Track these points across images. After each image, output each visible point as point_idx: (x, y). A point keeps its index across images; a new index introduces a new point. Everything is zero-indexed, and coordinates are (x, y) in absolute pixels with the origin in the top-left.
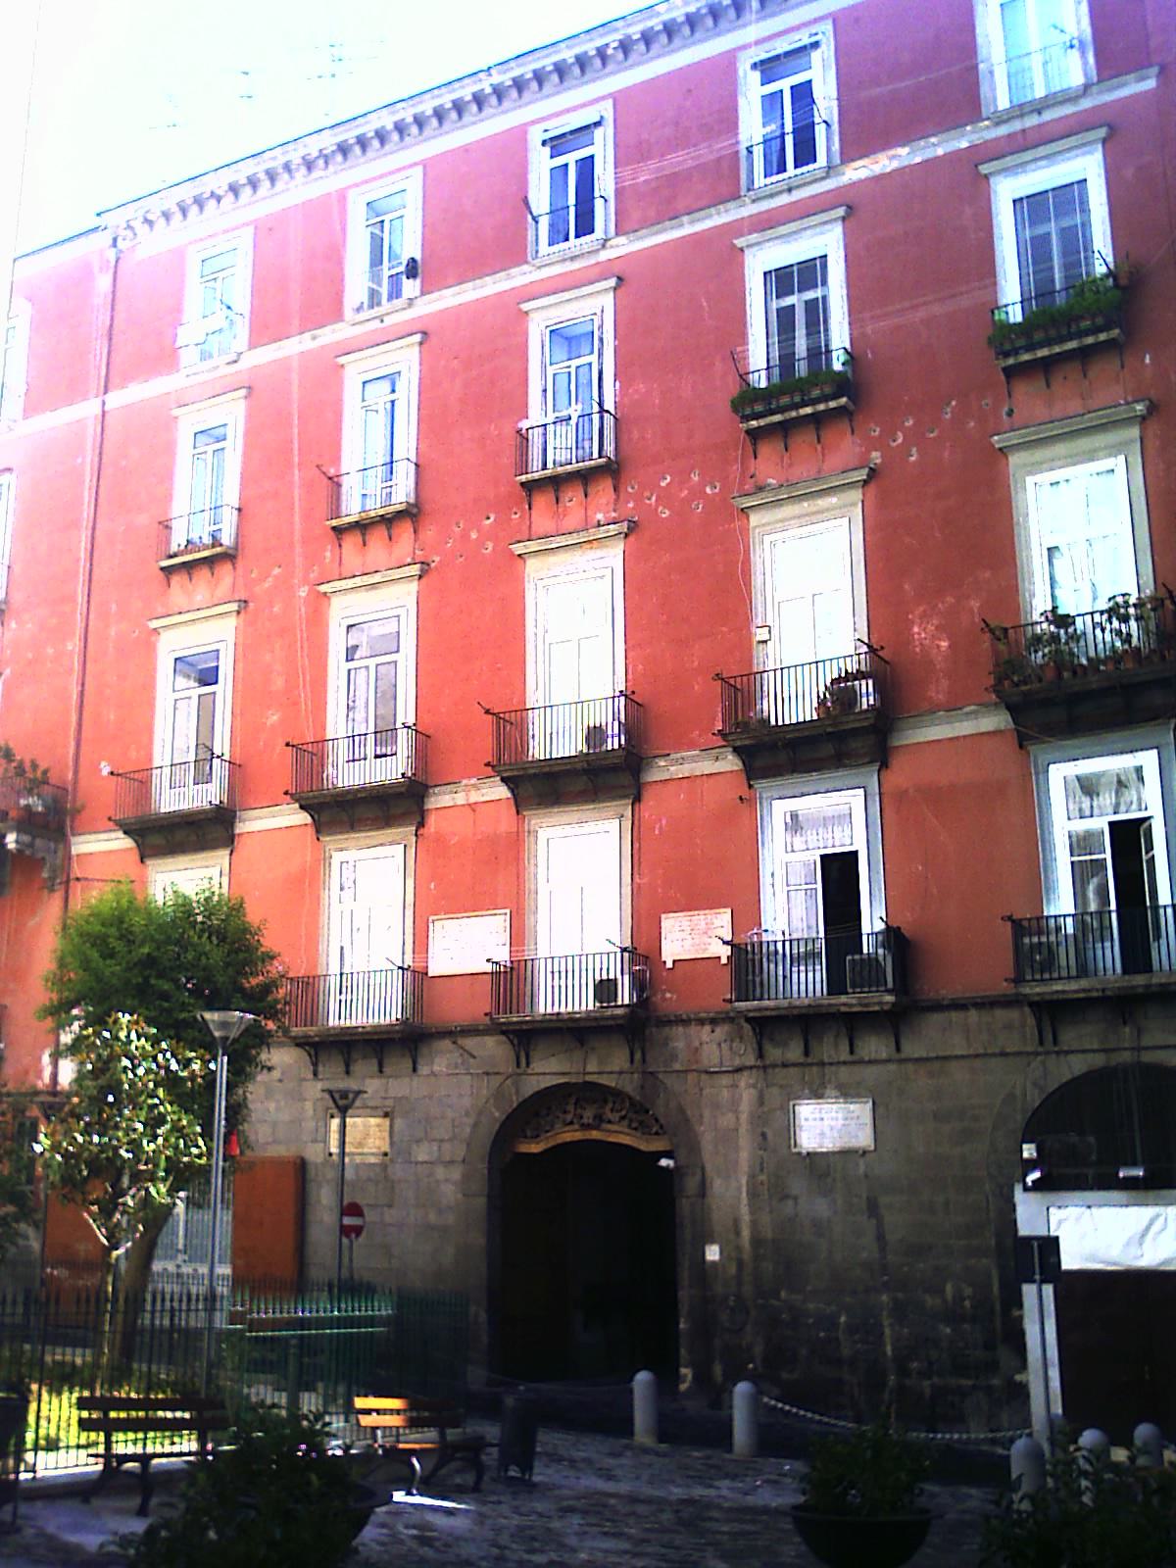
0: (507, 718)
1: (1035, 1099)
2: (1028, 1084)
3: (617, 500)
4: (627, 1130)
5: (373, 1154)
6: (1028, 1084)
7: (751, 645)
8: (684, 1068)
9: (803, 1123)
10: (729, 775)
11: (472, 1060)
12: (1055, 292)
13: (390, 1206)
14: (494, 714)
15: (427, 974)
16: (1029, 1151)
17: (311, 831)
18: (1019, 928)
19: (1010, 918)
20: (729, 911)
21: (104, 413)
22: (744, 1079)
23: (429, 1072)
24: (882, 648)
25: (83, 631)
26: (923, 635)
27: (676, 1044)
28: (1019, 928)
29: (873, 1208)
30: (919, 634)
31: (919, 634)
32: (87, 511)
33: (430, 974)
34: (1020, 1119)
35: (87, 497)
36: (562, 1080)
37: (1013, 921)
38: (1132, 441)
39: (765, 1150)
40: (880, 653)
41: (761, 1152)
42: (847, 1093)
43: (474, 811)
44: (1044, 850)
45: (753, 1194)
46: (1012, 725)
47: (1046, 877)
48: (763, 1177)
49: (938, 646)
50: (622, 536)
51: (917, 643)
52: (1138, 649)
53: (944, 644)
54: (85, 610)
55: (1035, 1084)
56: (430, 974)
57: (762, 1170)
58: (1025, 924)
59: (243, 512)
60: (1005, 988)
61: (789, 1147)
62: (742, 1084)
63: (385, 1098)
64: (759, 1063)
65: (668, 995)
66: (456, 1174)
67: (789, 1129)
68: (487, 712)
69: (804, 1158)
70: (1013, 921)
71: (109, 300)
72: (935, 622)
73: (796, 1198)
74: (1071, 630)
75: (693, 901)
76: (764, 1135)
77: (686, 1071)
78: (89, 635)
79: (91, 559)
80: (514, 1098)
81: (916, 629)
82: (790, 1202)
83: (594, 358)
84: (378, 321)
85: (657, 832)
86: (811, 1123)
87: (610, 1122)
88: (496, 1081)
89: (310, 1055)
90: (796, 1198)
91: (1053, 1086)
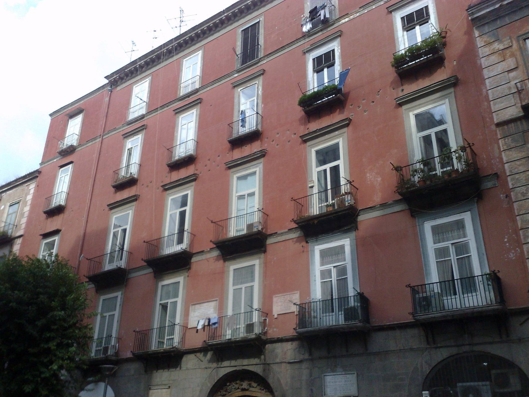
1: (427, 370)
2: (424, 363)
3: (261, 144)
4: (260, 391)
6: (424, 363)
8: (280, 361)
9: (328, 384)
11: (201, 362)
12: (175, 324)
15: (187, 327)
18: (414, 290)
20: (298, 292)
21: (345, 179)
22: (304, 365)
23: (186, 368)
24: (353, 181)
25: (87, 212)
26: (371, 177)
27: (277, 351)
28: (414, 290)
30: (369, 177)
31: (369, 177)
33: (189, 327)
36: (234, 369)
37: (411, 287)
40: (352, 183)
42: (346, 370)
43: (208, 261)
44: (424, 258)
49: (377, 181)
51: (369, 180)
52: (457, 170)
53: (379, 179)
54: (89, 205)
55: (426, 362)
56: (189, 327)
58: (416, 288)
60: (410, 319)
64: (310, 358)
65: (275, 330)
70: (411, 287)
71: (108, 104)
76: (312, 390)
77: (281, 363)
80: (216, 378)
81: (368, 175)
84: (489, 286)
85: (272, 263)
86: (332, 384)
87: (253, 387)
88: (210, 371)
91: (434, 363)
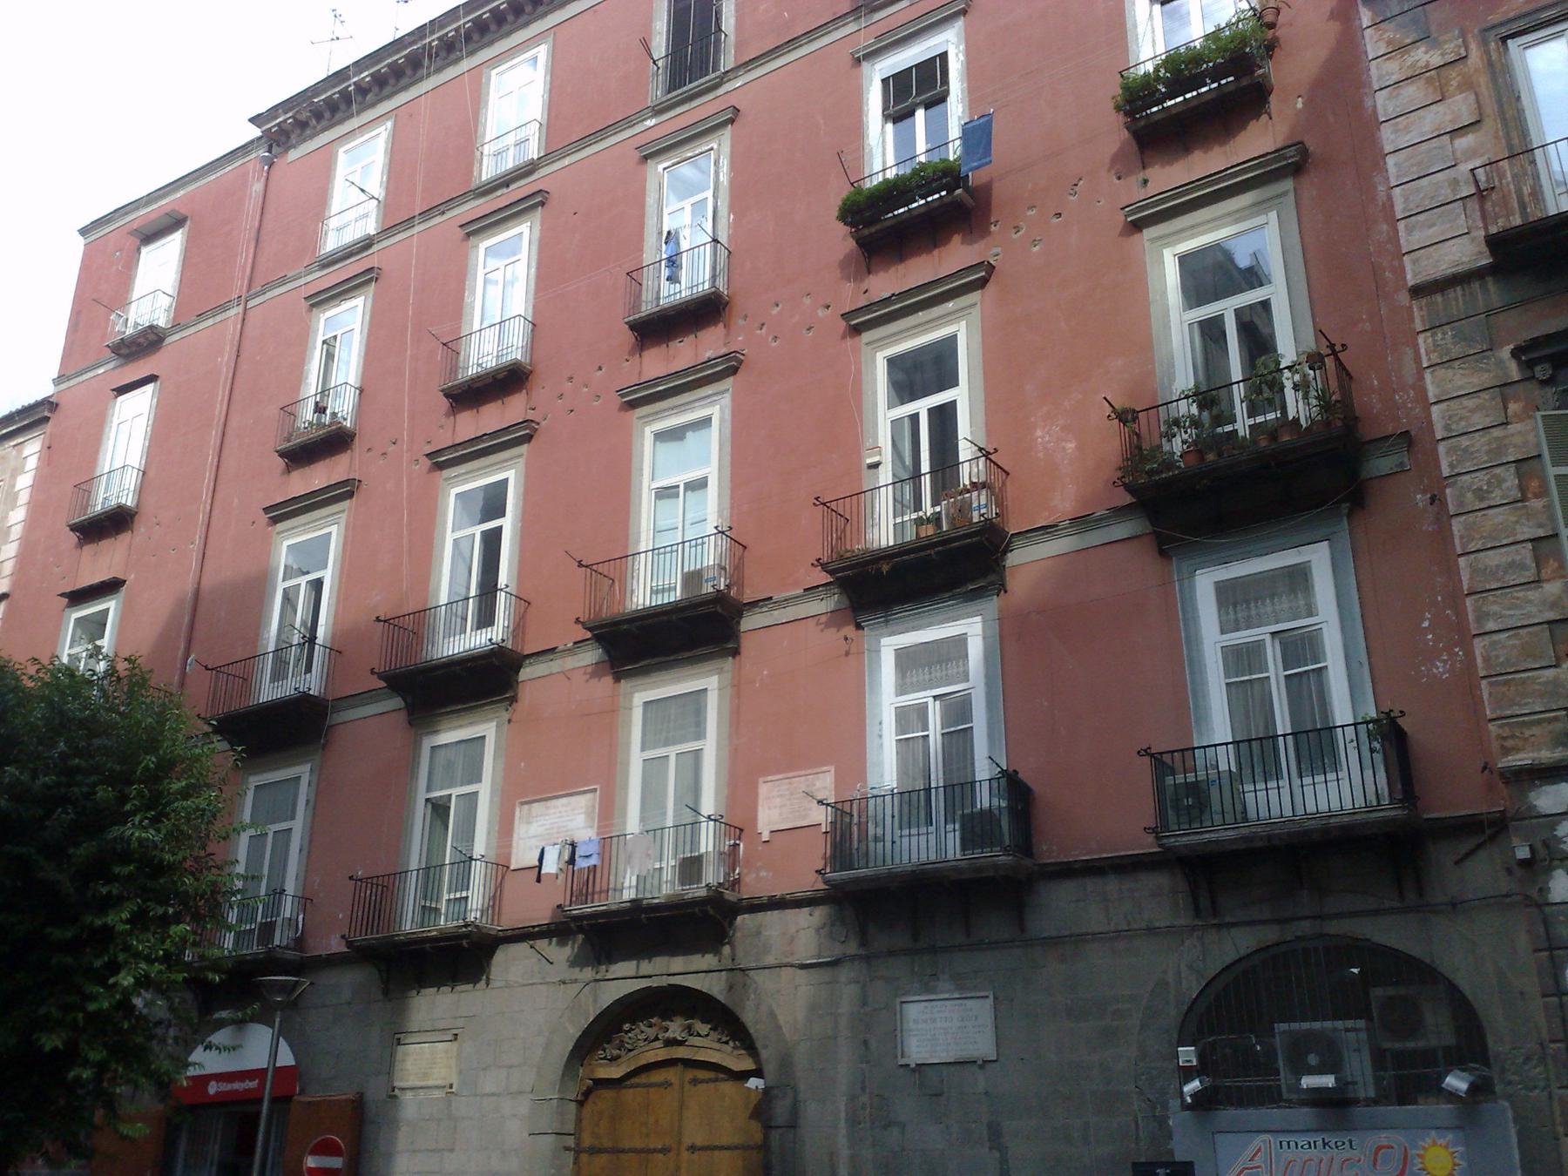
0: (600, 570)
1: (1192, 987)
3: (727, 335)
5: (437, 1087)
7: (859, 471)
9: (912, 1025)
10: (394, 714)
13: (452, 1150)
14: (587, 567)
16: (1187, 1054)
17: (403, 716)
18: (1160, 764)
19: (1146, 752)
28: (1160, 764)
29: (995, 1135)
31: (1042, 437)
32: (219, 410)
34: (1173, 1014)
35: (221, 394)
37: (1152, 755)
38: (1285, 194)
39: (868, 1062)
41: (864, 1065)
45: (853, 1122)
46: (1149, 529)
47: (1196, 706)
48: (864, 1099)
49: (1064, 448)
50: (174, 689)
51: (1040, 448)
52: (1296, 420)
54: (208, 508)
55: (1190, 967)
57: (863, 1089)
59: (364, 393)
60: (1148, 845)
61: (896, 1057)
62: (843, 979)
63: (455, 1018)
65: (763, 874)
66: (524, 1106)
67: (894, 1037)
68: (580, 565)
69: (913, 1070)
72: (1061, 422)
73: (903, 1126)
74: (1215, 411)
75: (792, 760)
78: (513, 201)
79: (219, 457)
80: (591, 1009)
82: (895, 1131)
83: (709, 194)
89: (380, 971)
90: (903, 1126)
